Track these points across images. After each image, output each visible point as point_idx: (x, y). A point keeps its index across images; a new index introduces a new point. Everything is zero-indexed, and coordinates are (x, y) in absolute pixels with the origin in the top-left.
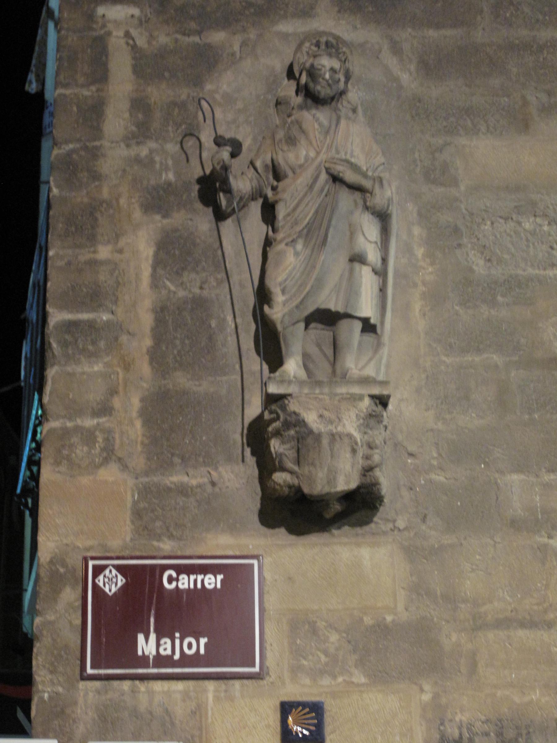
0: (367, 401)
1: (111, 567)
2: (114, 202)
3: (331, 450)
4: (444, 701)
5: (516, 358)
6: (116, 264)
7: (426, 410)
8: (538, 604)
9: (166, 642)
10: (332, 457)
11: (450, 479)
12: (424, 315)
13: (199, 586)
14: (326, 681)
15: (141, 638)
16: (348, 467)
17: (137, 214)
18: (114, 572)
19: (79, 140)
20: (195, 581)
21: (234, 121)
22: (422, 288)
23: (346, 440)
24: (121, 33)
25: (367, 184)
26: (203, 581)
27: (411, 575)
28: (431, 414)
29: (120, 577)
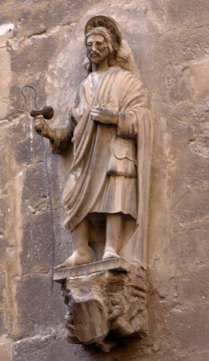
0: (107, 275)
3: (88, 312)
6: (4, 201)
10: (90, 316)
11: (184, 310)
12: (169, 196)
16: (100, 321)
17: (14, 166)
21: (64, 86)
23: (95, 304)
25: (114, 121)
28: (173, 267)
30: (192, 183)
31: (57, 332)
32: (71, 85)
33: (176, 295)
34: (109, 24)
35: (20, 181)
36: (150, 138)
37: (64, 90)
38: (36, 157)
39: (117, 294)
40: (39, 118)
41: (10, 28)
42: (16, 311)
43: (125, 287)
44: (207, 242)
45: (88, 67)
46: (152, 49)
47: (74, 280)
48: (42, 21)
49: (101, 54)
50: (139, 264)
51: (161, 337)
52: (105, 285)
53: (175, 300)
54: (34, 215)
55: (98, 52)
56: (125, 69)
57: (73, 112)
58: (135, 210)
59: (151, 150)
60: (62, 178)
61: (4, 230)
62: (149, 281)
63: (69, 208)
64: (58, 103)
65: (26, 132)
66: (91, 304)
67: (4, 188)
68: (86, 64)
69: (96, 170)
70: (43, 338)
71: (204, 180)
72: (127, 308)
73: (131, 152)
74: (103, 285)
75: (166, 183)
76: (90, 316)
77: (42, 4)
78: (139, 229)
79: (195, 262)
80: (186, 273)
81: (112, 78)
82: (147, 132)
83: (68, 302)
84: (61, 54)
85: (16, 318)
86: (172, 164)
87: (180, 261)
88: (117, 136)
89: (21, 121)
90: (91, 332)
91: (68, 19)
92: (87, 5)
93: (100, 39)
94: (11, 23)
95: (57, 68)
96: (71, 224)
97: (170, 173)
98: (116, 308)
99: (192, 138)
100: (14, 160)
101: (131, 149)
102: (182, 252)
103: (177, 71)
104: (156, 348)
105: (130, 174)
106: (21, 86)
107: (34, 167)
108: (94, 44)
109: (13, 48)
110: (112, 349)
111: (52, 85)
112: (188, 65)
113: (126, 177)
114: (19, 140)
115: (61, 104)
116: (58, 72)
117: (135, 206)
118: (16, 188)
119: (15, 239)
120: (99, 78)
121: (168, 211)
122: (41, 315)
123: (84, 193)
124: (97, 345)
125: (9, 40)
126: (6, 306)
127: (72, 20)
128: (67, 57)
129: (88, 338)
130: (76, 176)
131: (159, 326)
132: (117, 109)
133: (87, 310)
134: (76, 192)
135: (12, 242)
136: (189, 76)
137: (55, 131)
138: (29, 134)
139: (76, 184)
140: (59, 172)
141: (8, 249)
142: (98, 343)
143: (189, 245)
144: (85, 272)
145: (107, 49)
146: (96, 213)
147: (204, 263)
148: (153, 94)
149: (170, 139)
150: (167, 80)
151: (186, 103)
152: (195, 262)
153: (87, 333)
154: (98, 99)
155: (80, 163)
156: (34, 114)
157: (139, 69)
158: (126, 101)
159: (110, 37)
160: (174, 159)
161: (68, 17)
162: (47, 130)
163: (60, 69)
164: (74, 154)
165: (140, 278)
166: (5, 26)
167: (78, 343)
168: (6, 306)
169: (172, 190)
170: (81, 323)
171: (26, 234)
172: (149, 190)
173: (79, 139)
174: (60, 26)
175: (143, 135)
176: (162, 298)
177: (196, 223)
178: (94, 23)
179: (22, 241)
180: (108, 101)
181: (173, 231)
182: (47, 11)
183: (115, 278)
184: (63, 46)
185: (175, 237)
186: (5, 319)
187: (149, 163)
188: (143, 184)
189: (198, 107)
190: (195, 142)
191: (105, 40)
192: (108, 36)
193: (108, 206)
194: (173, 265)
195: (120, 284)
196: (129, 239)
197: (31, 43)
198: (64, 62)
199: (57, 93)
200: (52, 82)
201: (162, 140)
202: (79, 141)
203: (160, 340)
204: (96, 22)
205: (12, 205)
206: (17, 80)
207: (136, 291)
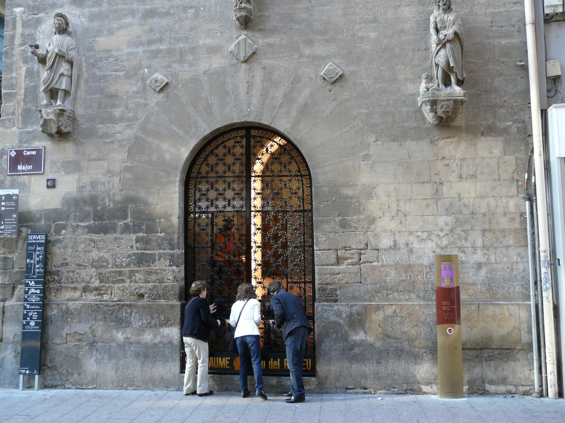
0: (58, 111)
4: (80, 178)
9: (24, 167)
14: (56, 174)
15: (19, 166)
17: (22, 65)
19: (9, 46)
21: (44, 38)
22: (84, 79)
24: (19, 16)
32: (47, 38)
60: (41, 73)
62: (74, 115)
63: (44, 84)
69: (56, 72)
72: (64, 123)
93: (60, 22)
97: (84, 78)
100: (21, 63)
104: (75, 138)
106: (26, 34)
129: (49, 132)
131: (76, 131)
134: (47, 79)
136: (95, 43)
137: (39, 54)
140: (41, 70)
144: (49, 108)
146: (55, 88)
155: (49, 69)
156: (31, 46)
170: (46, 126)
173: (49, 59)
180: (62, 47)
187: (77, 73)
191: (62, 23)
192: (64, 22)
193: (60, 86)
207: (69, 118)
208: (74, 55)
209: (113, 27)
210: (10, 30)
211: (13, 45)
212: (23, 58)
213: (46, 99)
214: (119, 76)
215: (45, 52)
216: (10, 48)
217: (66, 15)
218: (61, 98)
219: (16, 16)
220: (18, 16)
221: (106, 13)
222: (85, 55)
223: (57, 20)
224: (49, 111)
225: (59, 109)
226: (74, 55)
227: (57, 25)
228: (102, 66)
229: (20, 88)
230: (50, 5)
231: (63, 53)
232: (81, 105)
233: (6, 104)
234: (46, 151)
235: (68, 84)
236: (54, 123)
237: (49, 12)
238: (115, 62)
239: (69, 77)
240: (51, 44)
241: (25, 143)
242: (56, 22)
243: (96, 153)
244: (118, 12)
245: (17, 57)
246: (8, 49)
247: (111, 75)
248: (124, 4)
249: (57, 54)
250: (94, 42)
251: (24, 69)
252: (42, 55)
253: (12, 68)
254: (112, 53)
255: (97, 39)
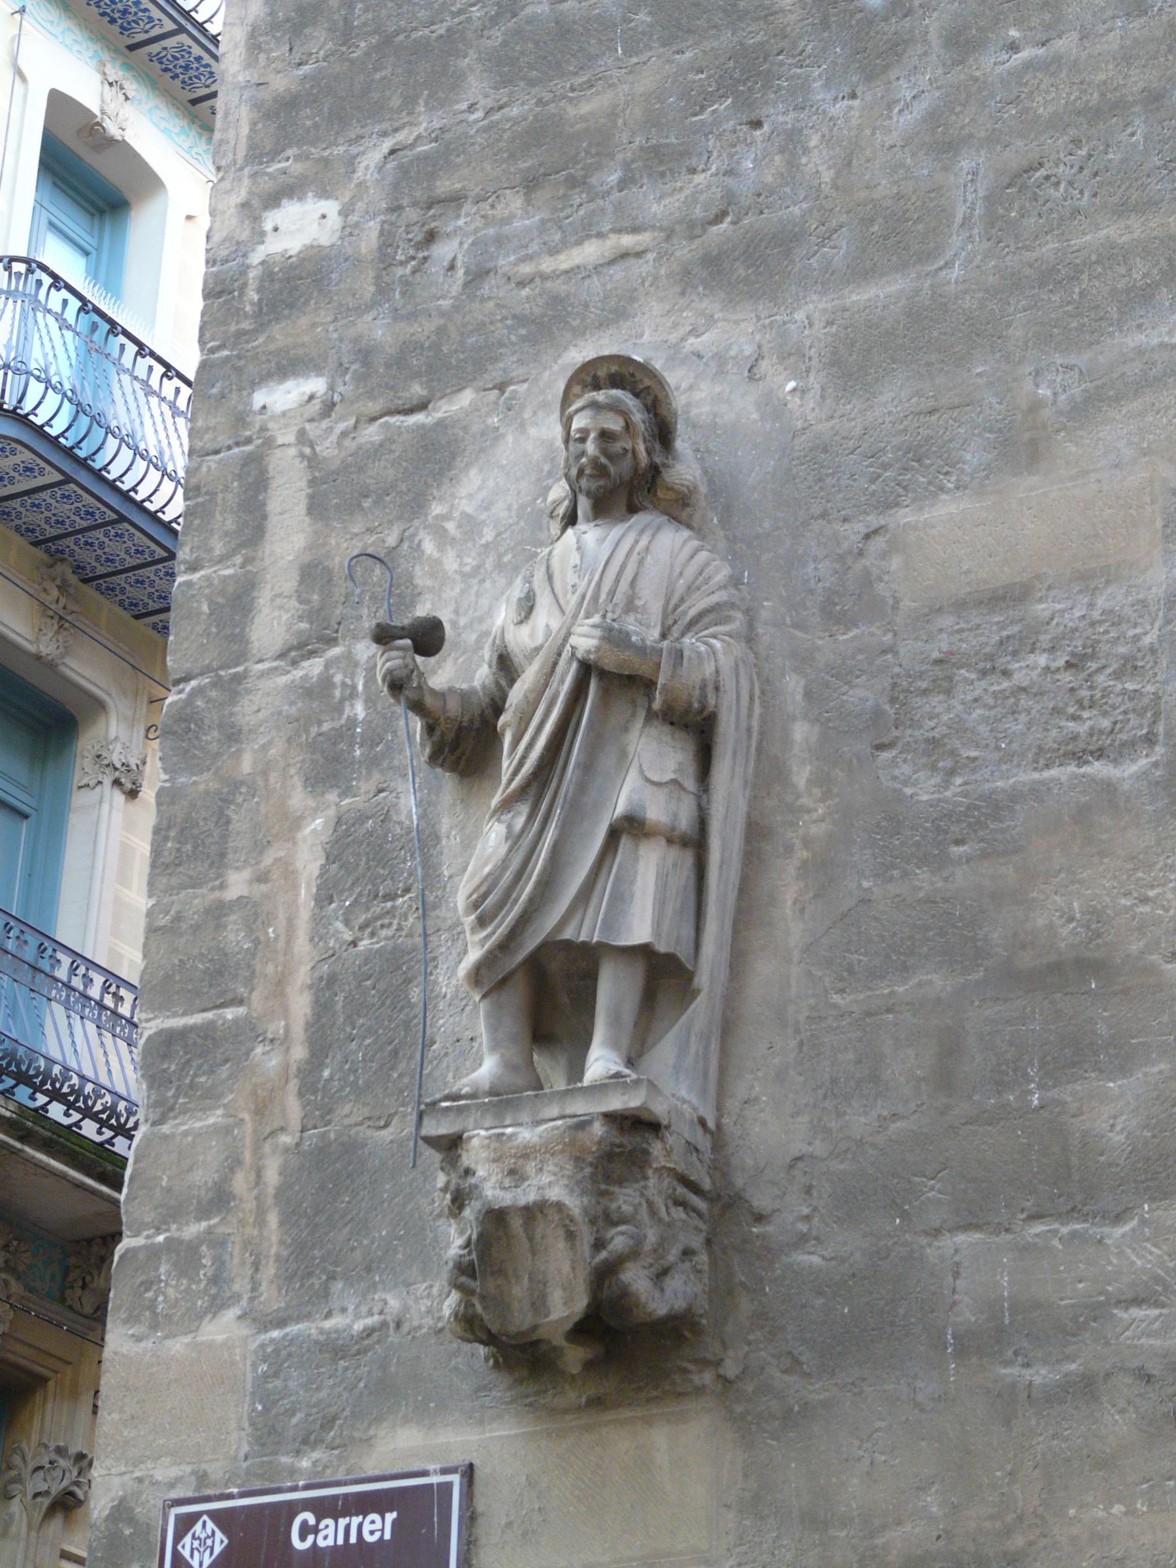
0: (598, 1129)
1: (205, 1517)
2: (260, 783)
5: (978, 975)
7: (793, 1117)
8: (991, 1517)
10: (534, 1252)
12: (802, 910)
13: (353, 1539)
16: (566, 1268)
17: (298, 799)
18: (210, 1525)
20: (347, 1528)
21: (477, 569)
22: (802, 854)
24: (290, 438)
25: (644, 670)
26: (360, 1526)
27: (745, 1476)
29: (219, 1535)
30: (877, 875)
31: (406, 1308)
32: (499, 566)
33: (806, 1211)
34: (641, 381)
35: (313, 845)
36: (749, 730)
37: (474, 581)
38: (369, 774)
39: (625, 1191)
40: (398, 649)
41: (314, 390)
42: (274, 1238)
43: (650, 1172)
44: (917, 1055)
45: (561, 511)
46: (770, 469)
47: (489, 1138)
48: (416, 375)
49: (612, 469)
50: (695, 1109)
51: (751, 1337)
52: (590, 1159)
53: (803, 1227)
54: (352, 950)
55: (603, 460)
56: (680, 522)
57: (509, 637)
58: (692, 945)
59: (751, 770)
60: (450, 842)
61: (252, 990)
62: (720, 1167)
63: (482, 922)
64: (453, 616)
65: (342, 700)
66: (539, 1216)
67: (258, 863)
68: (557, 503)
69: (576, 815)
70: (358, 1326)
71: (919, 868)
72: (652, 1236)
73: (691, 769)
74: (584, 1160)
75: (792, 870)
76: (534, 1252)
77: (421, 325)
78: (700, 1002)
79: (874, 1114)
80: (843, 1146)
81: (643, 542)
82: (744, 711)
83: (461, 1208)
84: (473, 472)
85: (272, 1260)
86: (815, 816)
87: (824, 1109)
88: (651, 716)
89: (327, 666)
90: (533, 1304)
91: (501, 372)
92: (569, 335)
93: (614, 424)
94: (317, 376)
95: (456, 514)
96: (483, 971)
97: (807, 842)
98: (622, 1233)
99: (886, 740)
100: (298, 782)
101: (691, 757)
102: (834, 1081)
103: (846, 538)
104: (730, 1369)
105: (685, 833)
106: (338, 562)
107: (361, 806)
108: (592, 435)
109: (318, 449)
110: (589, 1365)
111: (438, 562)
112: (883, 522)
113: (670, 841)
114: (320, 723)
115: (462, 621)
116: (460, 526)
117: (692, 933)
118: (299, 865)
119: (286, 1018)
120: (601, 541)
121: (796, 955)
122: (358, 1255)
123: (534, 878)
124: (544, 1347)
125: (308, 426)
126: (242, 1223)
127: (514, 374)
128: (491, 483)
129: (521, 1320)
130: (509, 827)
131: (745, 1305)
132: (655, 633)
133: (526, 1231)
134: (508, 875)
135: (276, 1028)
136: (884, 555)
137: (441, 695)
138: (352, 706)
139: (510, 851)
140: (445, 824)
141: (259, 1050)
142: (549, 1342)
143: (859, 1062)
144: (525, 1117)
145: (630, 455)
146: (568, 945)
147: (903, 1118)
148: (765, 604)
149: (814, 739)
150: (812, 565)
151: (872, 635)
152: (874, 1114)
153: (516, 1305)
154: (595, 597)
155: (523, 790)
156: (384, 636)
157: (723, 528)
158: (685, 613)
159: (644, 422)
160: (822, 800)
161: (501, 365)
162: (420, 687)
163: (466, 516)
164: (505, 763)
165: (695, 1154)
166: (298, 385)
167: (484, 1337)
168: (242, 1223)
169: (811, 894)
170: (501, 1272)
171: (322, 1007)
172: (736, 891)
173: (524, 720)
174: (478, 390)
175: (733, 718)
176: (759, 1218)
177: (882, 995)
178: (595, 377)
179: (308, 1026)
180: (630, 606)
181: (808, 1018)
182: (436, 347)
183: (625, 1140)
184: (483, 450)
185: (812, 1035)
186: (236, 1261)
187: (742, 806)
188: (721, 867)
189: (908, 648)
190: (894, 752)
191: (628, 426)
192: (639, 417)
193: (609, 924)
194: (804, 1119)
195: (637, 1161)
196: (667, 1032)
197: (377, 439)
198: (481, 495)
199: (452, 589)
200: (436, 555)
201: (787, 741)
202: (523, 725)
203: (746, 1348)
204: (602, 373)
205: (281, 916)
206: (324, 545)
207: (681, 1190)
208: (726, 663)
209: (1036, 406)
210: (219, 547)
211: (241, 656)
212: (313, 746)
213: (495, 1047)
214: (1108, 788)
215: (483, 675)
216: (217, 683)
217: (658, 365)
218: (615, 1021)
219: (269, 443)
220: (286, 436)
221: (967, 303)
222: (803, 659)
223: (594, 405)
224: (527, 1135)
225: (612, 1118)
226: (726, 663)
227: (591, 447)
228: (959, 727)
229: (280, 985)
230: (521, 320)
231: (642, 650)
232: (780, 1077)
233: (166, 1129)
234: (480, 1505)
235: (670, 909)
236: (571, 1236)
237: (518, 372)
238: (1067, 677)
239: (684, 842)
240: (544, 602)
241: (307, 1442)
242: (578, 423)
243: (932, 1502)
244: (1074, 278)
245: (265, 748)
246: (198, 692)
247: (1037, 791)
248: (1122, 210)
249: (586, 669)
250: (879, 543)
251: (317, 827)
252: (465, 696)
253: (224, 838)
254: (1041, 609)
255: (904, 516)
